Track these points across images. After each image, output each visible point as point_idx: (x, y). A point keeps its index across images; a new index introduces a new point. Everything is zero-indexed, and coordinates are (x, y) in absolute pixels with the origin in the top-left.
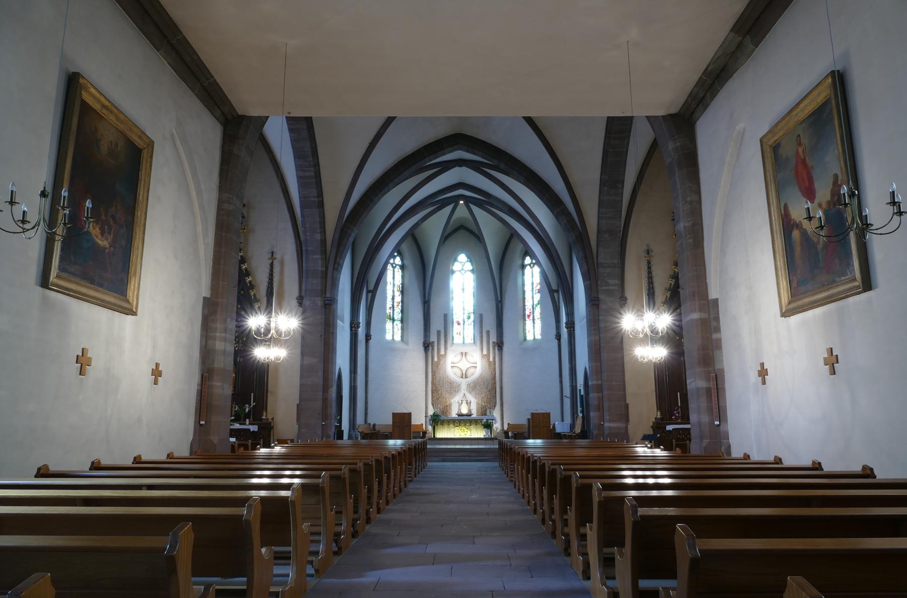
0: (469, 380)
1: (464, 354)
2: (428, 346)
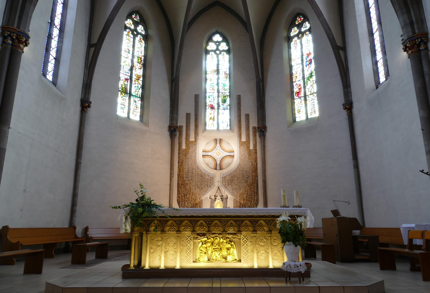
0: (225, 171)
1: (218, 141)
2: (175, 131)
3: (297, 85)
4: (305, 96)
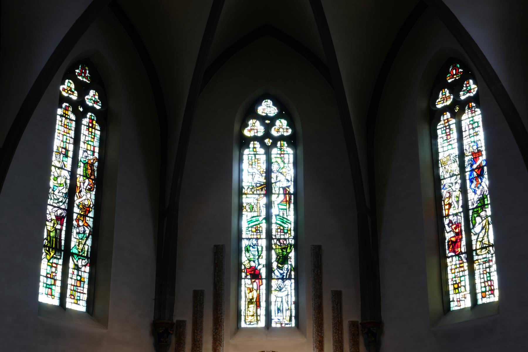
3: (453, 225)
4: (470, 251)
